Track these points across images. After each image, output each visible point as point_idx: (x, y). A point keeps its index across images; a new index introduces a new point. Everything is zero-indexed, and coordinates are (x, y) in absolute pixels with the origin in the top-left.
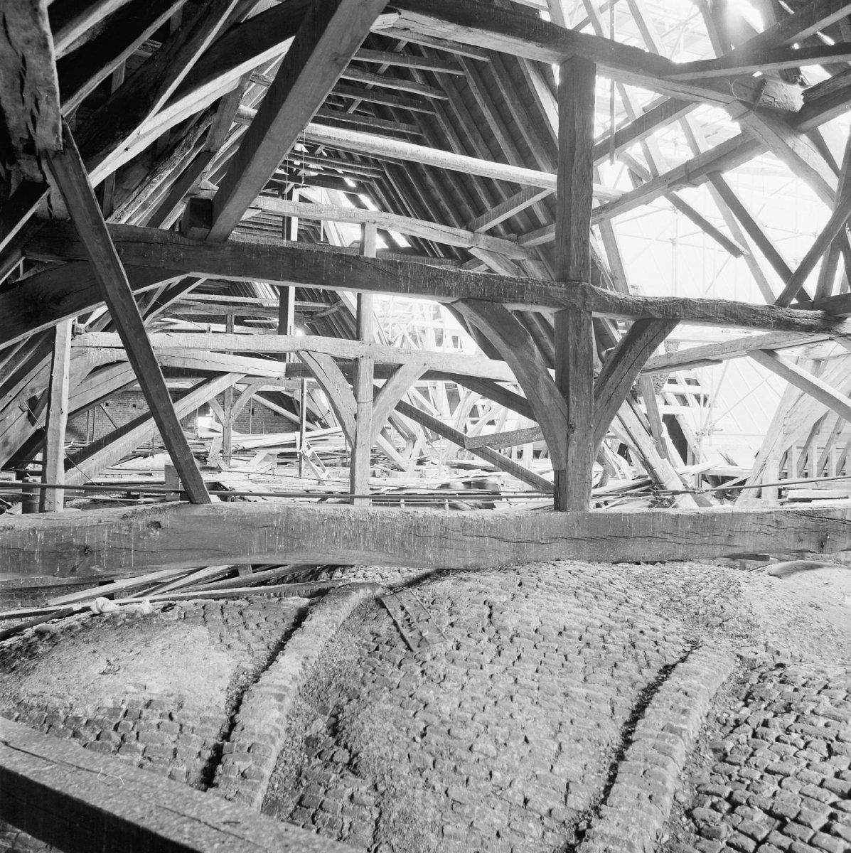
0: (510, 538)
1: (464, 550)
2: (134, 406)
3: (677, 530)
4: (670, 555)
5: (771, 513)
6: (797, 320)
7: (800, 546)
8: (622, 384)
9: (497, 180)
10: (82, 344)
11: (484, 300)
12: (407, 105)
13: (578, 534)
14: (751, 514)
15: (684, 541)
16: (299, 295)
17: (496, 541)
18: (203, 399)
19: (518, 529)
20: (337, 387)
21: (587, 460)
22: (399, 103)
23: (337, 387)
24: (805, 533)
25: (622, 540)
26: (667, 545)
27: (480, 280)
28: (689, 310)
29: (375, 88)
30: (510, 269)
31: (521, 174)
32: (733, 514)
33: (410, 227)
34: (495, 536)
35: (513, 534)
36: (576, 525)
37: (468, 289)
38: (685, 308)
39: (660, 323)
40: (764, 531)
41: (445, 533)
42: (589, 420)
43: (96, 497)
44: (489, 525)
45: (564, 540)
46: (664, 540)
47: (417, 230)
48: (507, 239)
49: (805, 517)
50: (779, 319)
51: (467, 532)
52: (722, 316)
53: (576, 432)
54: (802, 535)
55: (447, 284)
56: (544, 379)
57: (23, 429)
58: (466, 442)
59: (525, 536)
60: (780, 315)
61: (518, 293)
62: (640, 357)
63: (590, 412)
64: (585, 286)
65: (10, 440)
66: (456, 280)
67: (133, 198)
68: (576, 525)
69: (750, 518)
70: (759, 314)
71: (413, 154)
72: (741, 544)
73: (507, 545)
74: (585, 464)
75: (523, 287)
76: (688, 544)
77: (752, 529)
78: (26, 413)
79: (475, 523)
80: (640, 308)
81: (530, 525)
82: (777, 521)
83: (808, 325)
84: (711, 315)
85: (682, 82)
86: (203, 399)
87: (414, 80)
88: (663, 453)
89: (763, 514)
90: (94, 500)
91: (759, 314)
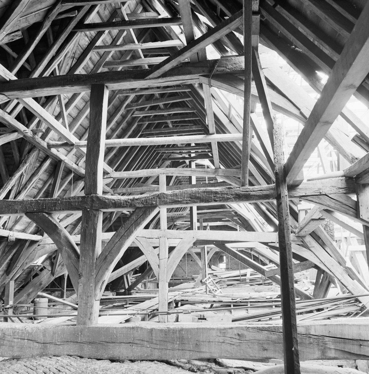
0: (39, 341)
1: (13, 347)
2: (192, 260)
3: (152, 339)
4: (148, 356)
5: (232, 328)
6: (252, 193)
7: (265, 354)
8: (115, 248)
9: (231, 142)
10: (44, 243)
11: (34, 212)
12: (185, 118)
13: (81, 340)
14: (214, 329)
15: (158, 347)
16: (199, 208)
17: (31, 342)
18: (144, 260)
19: (44, 336)
20: (149, 252)
21: (89, 295)
22: (181, 118)
23: (149, 252)
24: (268, 344)
25: (111, 345)
26: (145, 349)
27: (33, 203)
28: (163, 199)
29: (155, 116)
30: (237, 182)
31: (181, 139)
32: (197, 329)
33: (181, 173)
34: (31, 339)
35: (41, 338)
36: (80, 334)
37: (26, 208)
38: (160, 198)
39: (143, 209)
40: (227, 342)
41: (3, 337)
42: (91, 271)
43: (115, 304)
44: (28, 332)
45: (72, 343)
46: (142, 346)
47: (185, 173)
48: (234, 168)
49: (266, 332)
50: (236, 194)
51: (15, 337)
52: (188, 199)
53: (82, 278)
54: (266, 346)
55: (16, 207)
56: (66, 250)
57: (49, 278)
58: (265, 274)
59: (48, 340)
60: (237, 192)
61: (53, 206)
62: (128, 231)
63: (92, 266)
64: (93, 196)
65: (42, 283)
66: (20, 205)
67: (4, 186)
68: (80, 334)
69: (214, 332)
70: (219, 194)
71: (124, 143)
72: (207, 351)
73: (37, 345)
74: (88, 297)
75: (56, 203)
76: (162, 349)
77: (217, 340)
78: (50, 272)
79: (20, 331)
80: (129, 203)
81: (52, 333)
82: (239, 335)
83: (263, 195)
84: (180, 200)
85: (159, 77)
86: (144, 260)
87: (188, 107)
88: (353, 276)
89: (225, 329)
90: (114, 306)
91: (219, 194)
